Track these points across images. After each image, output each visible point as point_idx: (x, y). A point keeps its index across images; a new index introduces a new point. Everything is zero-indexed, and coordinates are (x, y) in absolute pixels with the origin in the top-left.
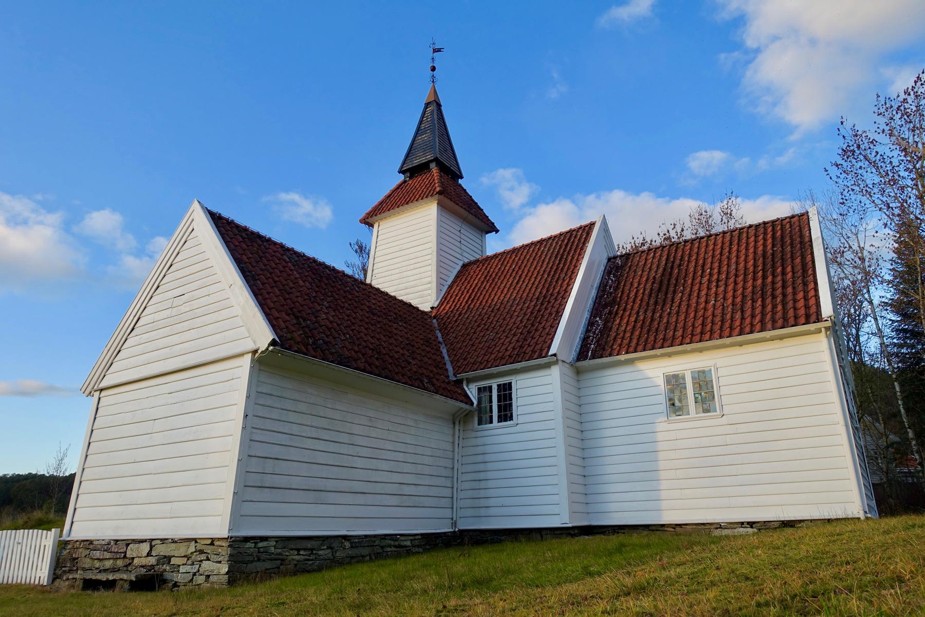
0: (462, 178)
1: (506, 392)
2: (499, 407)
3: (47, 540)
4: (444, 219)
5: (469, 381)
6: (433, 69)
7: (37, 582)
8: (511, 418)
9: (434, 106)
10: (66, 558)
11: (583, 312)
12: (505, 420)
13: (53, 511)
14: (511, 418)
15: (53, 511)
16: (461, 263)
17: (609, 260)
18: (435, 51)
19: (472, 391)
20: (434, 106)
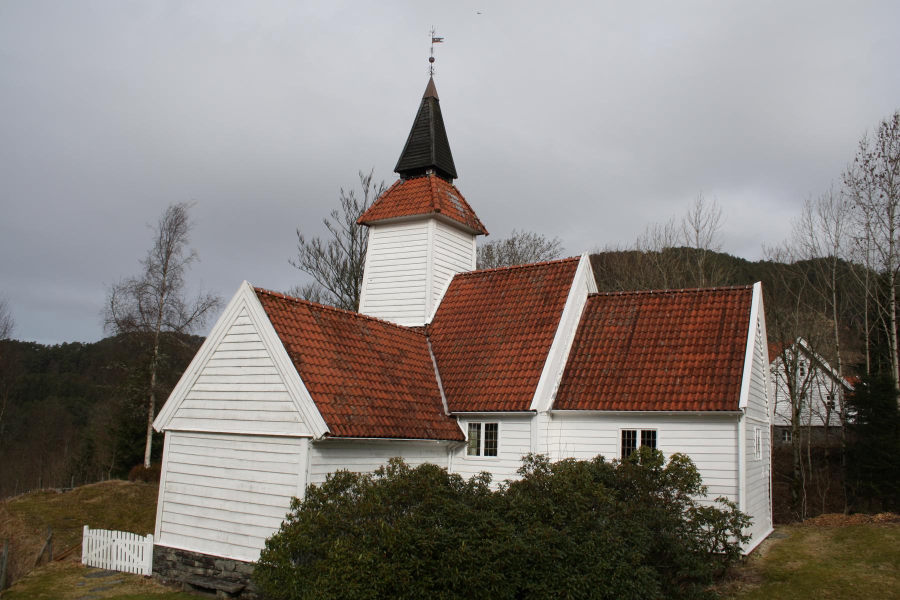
0: (456, 177)
1: (492, 431)
2: (486, 443)
3: (148, 543)
4: (440, 233)
5: (462, 418)
6: (432, 60)
7: (139, 573)
8: (495, 455)
9: (431, 86)
10: (160, 555)
11: (573, 324)
12: (491, 455)
13: (689, 496)
14: (495, 455)
15: (689, 496)
16: (453, 274)
17: (589, 297)
18: (436, 40)
19: (464, 426)
20: (431, 86)
